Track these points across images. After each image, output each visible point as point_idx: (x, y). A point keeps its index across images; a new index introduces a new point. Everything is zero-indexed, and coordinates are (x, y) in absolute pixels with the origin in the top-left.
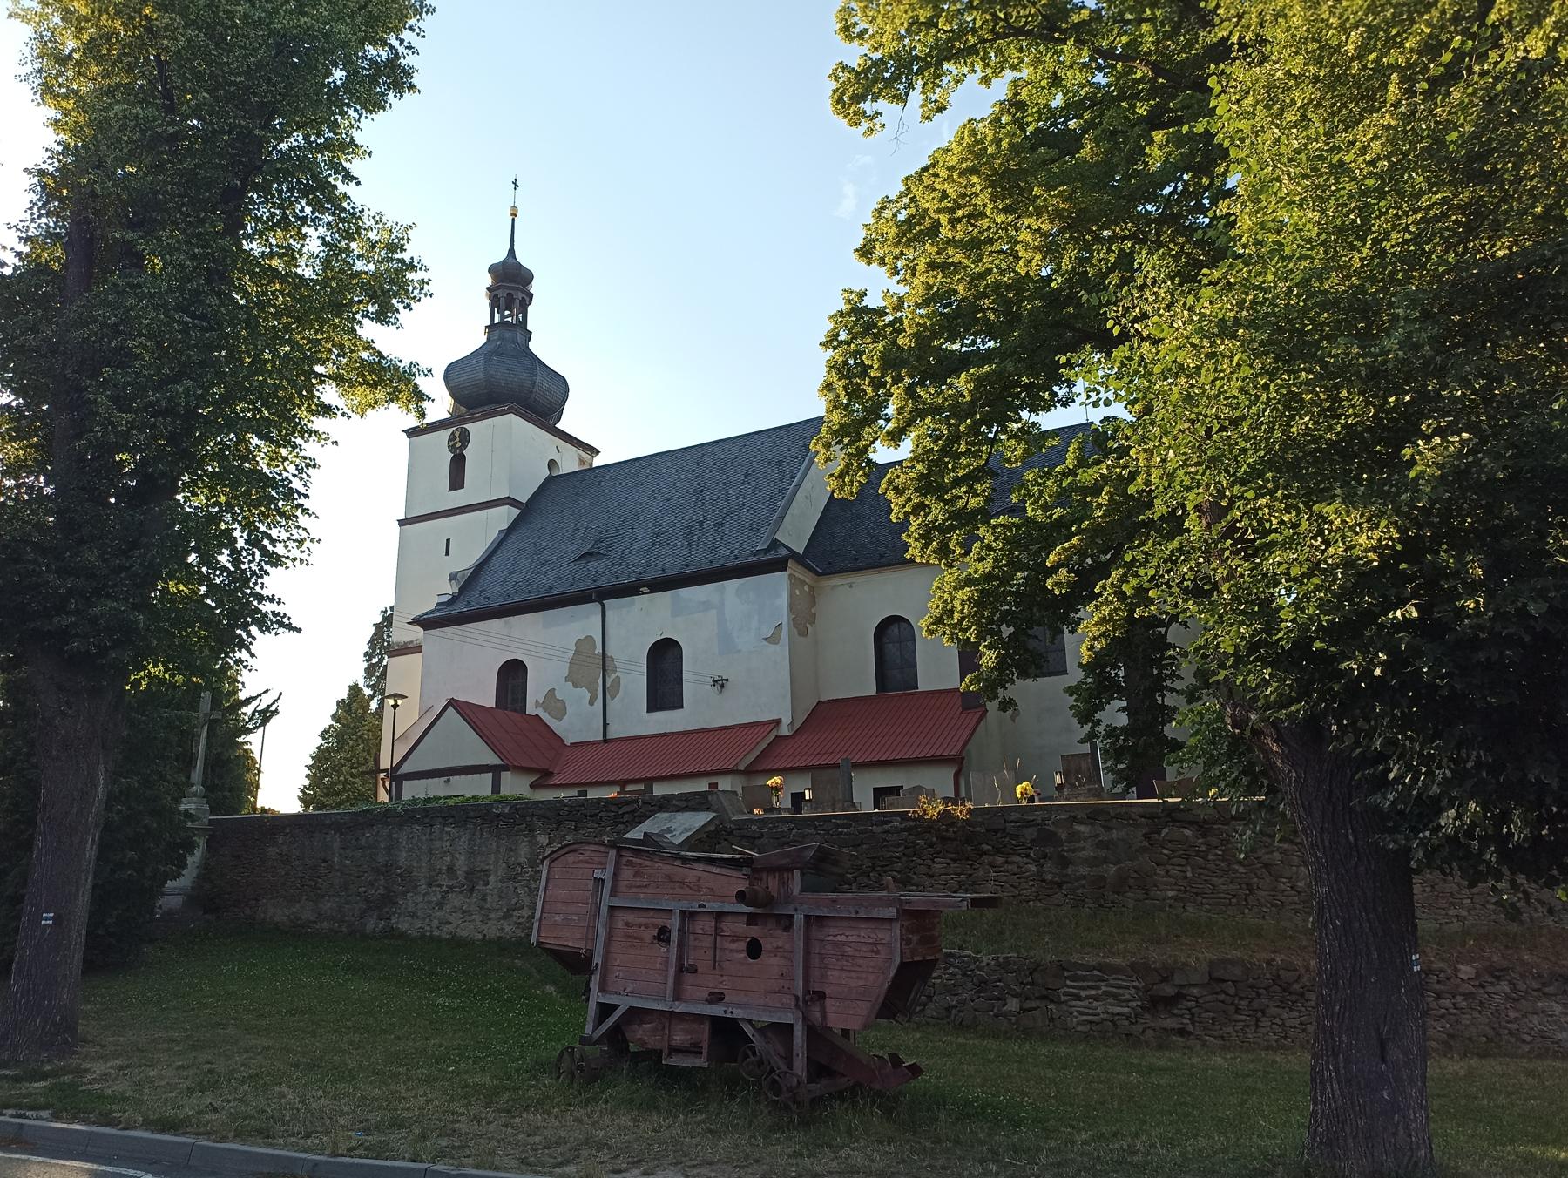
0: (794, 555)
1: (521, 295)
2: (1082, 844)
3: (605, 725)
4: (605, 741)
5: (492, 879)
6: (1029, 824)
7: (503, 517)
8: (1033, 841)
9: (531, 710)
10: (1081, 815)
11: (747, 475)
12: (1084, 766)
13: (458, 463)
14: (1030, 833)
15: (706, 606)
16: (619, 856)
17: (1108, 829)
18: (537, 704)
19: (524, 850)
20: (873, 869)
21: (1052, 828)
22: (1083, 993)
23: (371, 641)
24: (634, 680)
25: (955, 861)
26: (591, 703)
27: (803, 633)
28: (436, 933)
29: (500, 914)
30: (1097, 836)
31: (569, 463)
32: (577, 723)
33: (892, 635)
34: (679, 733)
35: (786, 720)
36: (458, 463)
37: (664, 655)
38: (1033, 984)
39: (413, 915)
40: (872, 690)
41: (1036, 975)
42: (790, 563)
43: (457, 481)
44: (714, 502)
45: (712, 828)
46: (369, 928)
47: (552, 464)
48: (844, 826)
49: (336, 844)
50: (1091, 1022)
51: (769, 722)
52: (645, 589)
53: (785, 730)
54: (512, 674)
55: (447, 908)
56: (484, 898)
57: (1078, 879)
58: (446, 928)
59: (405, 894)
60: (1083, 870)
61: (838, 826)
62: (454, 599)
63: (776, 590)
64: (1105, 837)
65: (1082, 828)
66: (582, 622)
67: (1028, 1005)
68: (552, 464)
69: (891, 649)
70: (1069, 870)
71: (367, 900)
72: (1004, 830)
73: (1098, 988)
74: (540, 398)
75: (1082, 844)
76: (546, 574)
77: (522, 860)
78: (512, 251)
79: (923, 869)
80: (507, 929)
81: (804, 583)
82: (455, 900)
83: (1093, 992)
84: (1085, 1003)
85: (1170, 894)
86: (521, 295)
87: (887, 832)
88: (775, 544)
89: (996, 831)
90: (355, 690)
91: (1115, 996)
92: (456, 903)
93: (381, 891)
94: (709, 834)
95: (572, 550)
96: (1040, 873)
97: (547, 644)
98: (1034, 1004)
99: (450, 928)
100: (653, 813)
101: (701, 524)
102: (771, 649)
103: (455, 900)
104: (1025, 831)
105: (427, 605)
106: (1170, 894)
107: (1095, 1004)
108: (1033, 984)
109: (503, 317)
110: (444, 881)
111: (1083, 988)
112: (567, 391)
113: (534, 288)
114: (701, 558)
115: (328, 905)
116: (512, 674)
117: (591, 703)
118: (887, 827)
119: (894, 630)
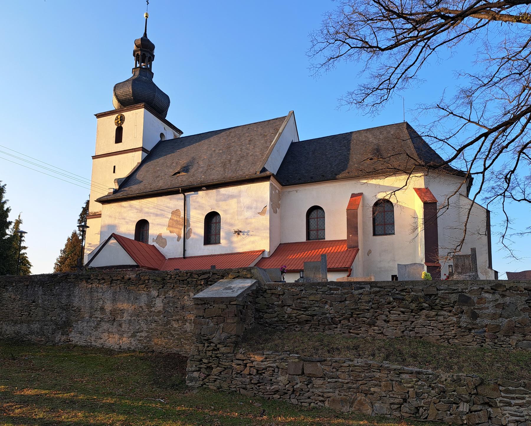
0: (273, 175)
1: (149, 55)
2: (487, 305)
4: (184, 258)
6: (453, 291)
7: (138, 157)
8: (455, 302)
9: (151, 242)
11: (250, 141)
12: (467, 262)
13: (119, 132)
17: (503, 296)
19: (144, 298)
20: (352, 316)
21: (468, 295)
22: (513, 402)
23: (81, 215)
24: (198, 228)
25: (403, 312)
26: (178, 240)
27: (275, 212)
29: (130, 334)
30: (497, 300)
31: (170, 135)
33: (315, 213)
34: (218, 255)
36: (119, 132)
37: (212, 219)
39: (81, 333)
40: (303, 239)
41: (479, 389)
42: (272, 178)
43: (119, 139)
47: (162, 135)
49: (40, 293)
51: (260, 251)
52: (204, 188)
53: (266, 255)
54: (142, 226)
55: (100, 330)
56: (120, 325)
57: (482, 327)
59: (77, 321)
60: (487, 321)
61: (331, 289)
62: (115, 191)
64: (501, 301)
65: (487, 295)
66: (174, 202)
67: (474, 408)
68: (162, 135)
70: (479, 320)
71: (56, 324)
72: (436, 295)
73: (523, 398)
75: (487, 305)
77: (142, 304)
78: (145, 34)
80: (134, 343)
81: (276, 189)
82: (105, 326)
83: (520, 401)
84: (515, 408)
86: (149, 55)
89: (430, 296)
90: (74, 235)
93: (64, 319)
94: (253, 291)
95: (172, 171)
96: (458, 322)
97: (160, 215)
99: (102, 341)
101: (230, 161)
104: (450, 295)
108: (477, 394)
109: (141, 65)
110: (98, 314)
111: (513, 398)
112: (169, 102)
113: (156, 53)
114: (230, 175)
115: (36, 326)
116: (142, 226)
117: (178, 240)
118: (361, 291)
119: (314, 214)
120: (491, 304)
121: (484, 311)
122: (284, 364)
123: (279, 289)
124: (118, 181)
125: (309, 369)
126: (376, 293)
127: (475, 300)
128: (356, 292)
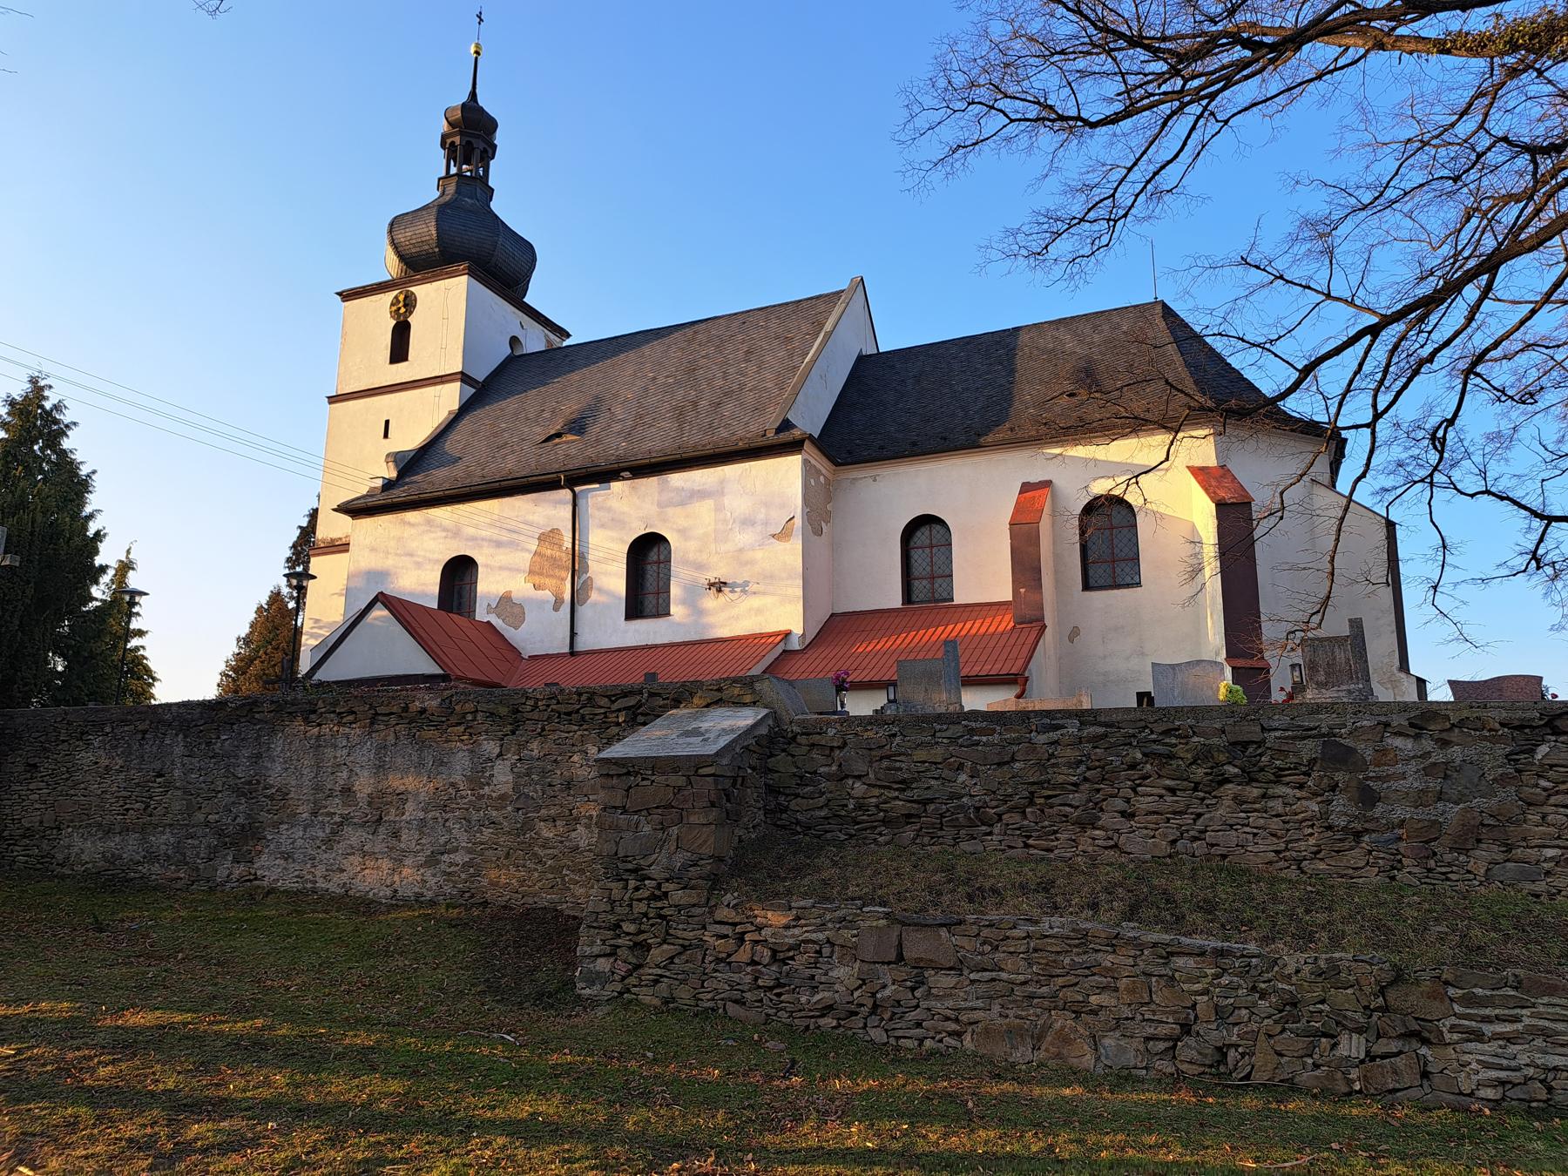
1: (482, 145)
2: (1399, 768)
3: (573, 634)
4: (573, 653)
5: (410, 806)
6: (1307, 733)
7: (450, 397)
9: (481, 615)
10: (1398, 721)
11: (747, 352)
12: (1340, 656)
14: (1309, 749)
15: (702, 494)
16: (1478, 375)
17: (1445, 743)
18: (489, 610)
20: (1032, 803)
22: (1488, 1029)
23: (294, 546)
24: (610, 577)
27: (818, 532)
28: (321, 884)
29: (421, 859)
30: (1427, 755)
32: (540, 634)
33: (925, 536)
35: (798, 629)
37: (647, 553)
38: (1385, 1009)
39: (287, 857)
40: (895, 601)
42: (807, 445)
43: (399, 351)
44: (710, 381)
45: (764, 731)
46: (221, 873)
47: (514, 341)
48: (982, 732)
50: (1502, 1083)
51: (777, 634)
52: (626, 474)
53: (795, 645)
54: (459, 572)
55: (340, 848)
56: (396, 835)
57: (1391, 827)
58: (338, 879)
60: (1401, 812)
61: (972, 732)
62: (389, 485)
63: (785, 476)
64: (1438, 757)
65: (1398, 742)
66: (550, 510)
67: (1381, 1047)
68: (514, 341)
69: (919, 558)
70: (1379, 810)
71: (220, 834)
73: (1517, 1019)
74: (502, 266)
75: (1399, 768)
76: (504, 457)
78: (473, 95)
79: (1119, 804)
80: (432, 882)
81: (819, 472)
82: (354, 836)
84: (1493, 1047)
85: (1550, 853)
86: (482, 145)
87: (1056, 742)
88: (786, 425)
89: (1245, 745)
90: (276, 597)
91: (1545, 1034)
92: (354, 841)
94: (759, 739)
95: (540, 432)
96: (1325, 815)
98: (1394, 1047)
99: (344, 877)
100: (665, 708)
101: (695, 404)
102: (779, 546)
103: (354, 836)
105: (358, 488)
106: (1550, 853)
107: (1513, 1049)
110: (336, 806)
111: (1487, 1020)
113: (499, 138)
114: (694, 439)
115: (162, 841)
116: (459, 572)
118: (1054, 735)
119: (922, 536)
120: (1412, 767)
121: (1394, 785)
122: (847, 934)
123: (831, 732)
124: (395, 458)
125: (918, 946)
126: (1095, 740)
127: (1369, 754)
128: (1042, 738)
